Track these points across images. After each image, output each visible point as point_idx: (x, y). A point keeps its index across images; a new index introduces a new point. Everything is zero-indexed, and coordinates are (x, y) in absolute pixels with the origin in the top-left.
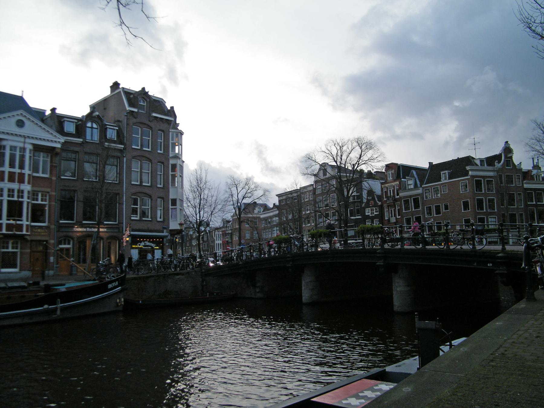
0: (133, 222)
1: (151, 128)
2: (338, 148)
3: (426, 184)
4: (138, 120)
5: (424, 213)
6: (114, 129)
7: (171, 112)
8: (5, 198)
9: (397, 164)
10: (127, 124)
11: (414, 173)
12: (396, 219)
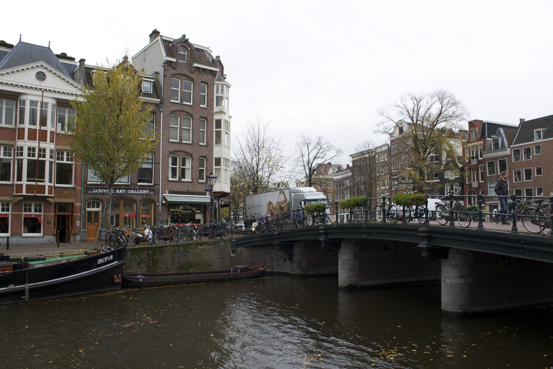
0: (172, 184)
1: (192, 80)
2: (416, 102)
3: (515, 144)
4: (178, 71)
5: (511, 177)
6: (151, 82)
7: (217, 62)
8: (25, 157)
9: (482, 121)
10: (165, 76)
11: (502, 131)
12: (479, 183)
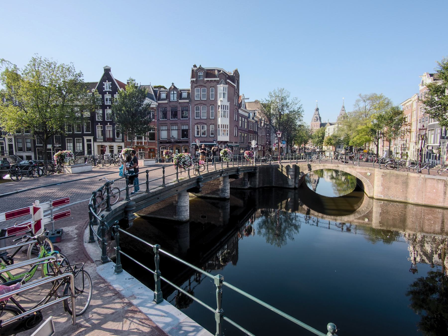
4: (198, 84)
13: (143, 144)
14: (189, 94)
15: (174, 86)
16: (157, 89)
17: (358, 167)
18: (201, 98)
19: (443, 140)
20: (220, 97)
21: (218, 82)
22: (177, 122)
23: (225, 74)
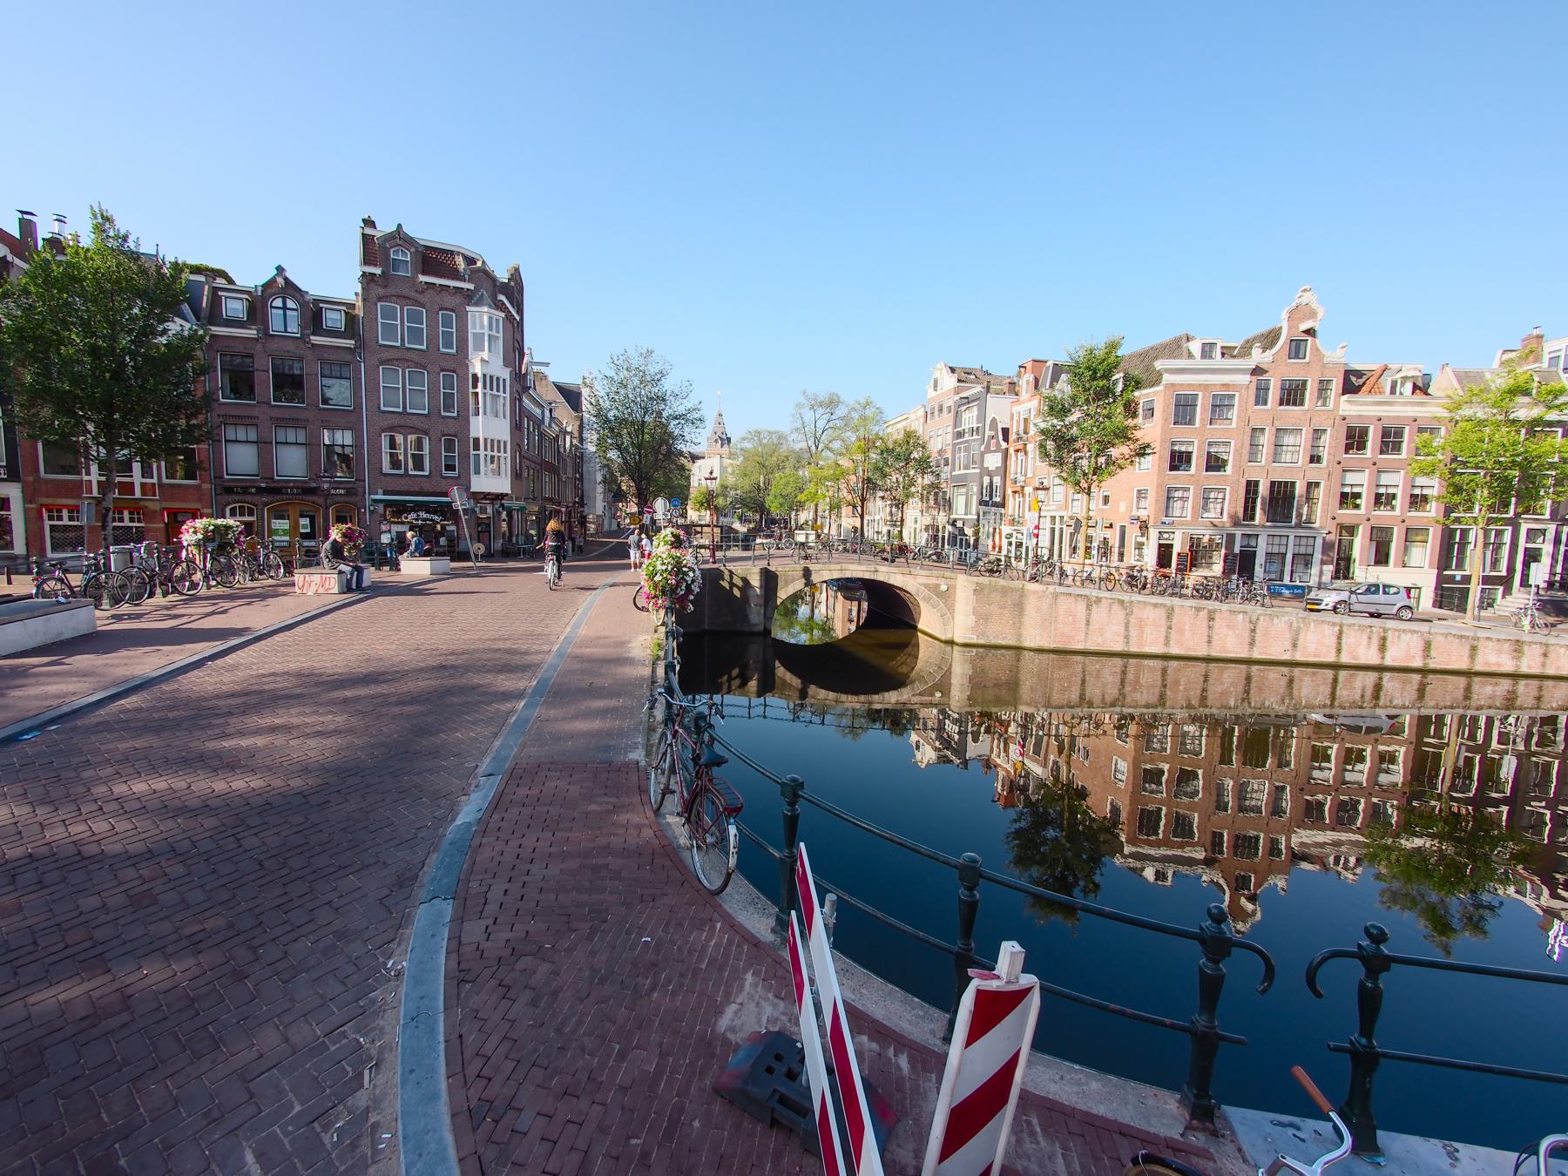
13: (138, 494)
14: (351, 319)
15: (286, 279)
16: (202, 278)
17: (918, 571)
18: (403, 340)
19: (983, 509)
20: (480, 348)
21: (469, 297)
22: (256, 412)
23: (486, 274)
